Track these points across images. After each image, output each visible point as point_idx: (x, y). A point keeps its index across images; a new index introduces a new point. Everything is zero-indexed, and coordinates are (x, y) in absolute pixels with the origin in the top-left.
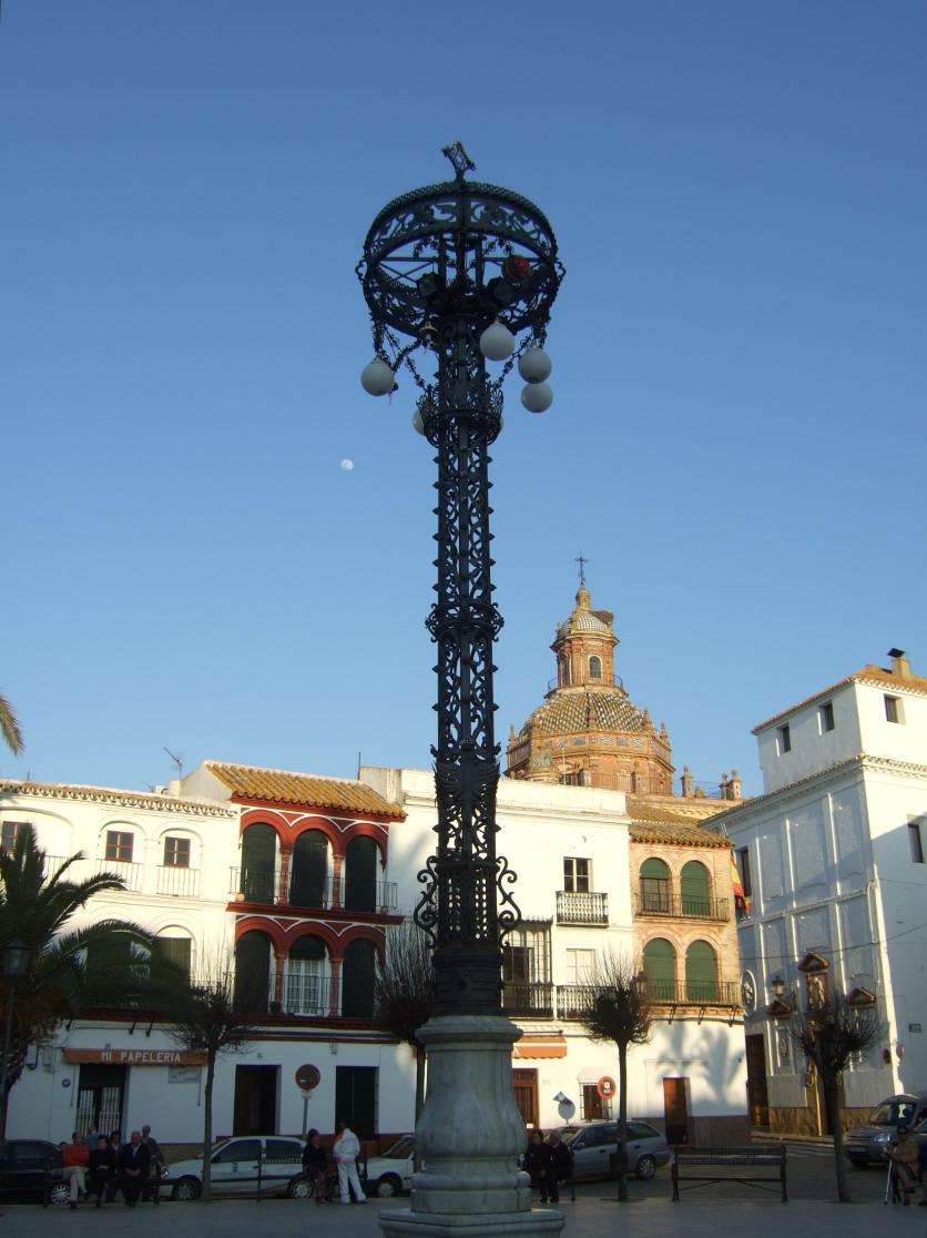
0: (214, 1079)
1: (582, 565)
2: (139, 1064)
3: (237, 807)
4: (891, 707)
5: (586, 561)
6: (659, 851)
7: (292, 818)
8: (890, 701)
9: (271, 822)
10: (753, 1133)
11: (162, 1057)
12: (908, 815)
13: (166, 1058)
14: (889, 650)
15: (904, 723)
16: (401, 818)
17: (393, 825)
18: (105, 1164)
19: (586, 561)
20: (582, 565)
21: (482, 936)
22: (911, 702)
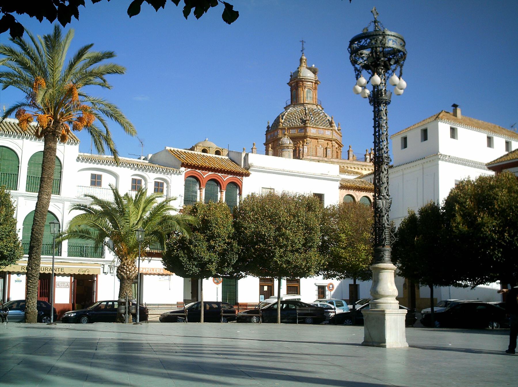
0: (281, 290)
1: (303, 44)
2: (146, 274)
3: (183, 169)
4: (453, 133)
5: (305, 42)
6: (351, 192)
7: (225, 177)
8: (490, 139)
9: (217, 179)
10: (284, 282)
11: (156, 271)
12: (456, 180)
13: (158, 271)
14: (452, 104)
15: (116, 56)
16: (247, 175)
17: (245, 179)
18: (110, 305)
19: (305, 42)
20: (303, 44)
21: (497, 259)
22: (461, 131)
